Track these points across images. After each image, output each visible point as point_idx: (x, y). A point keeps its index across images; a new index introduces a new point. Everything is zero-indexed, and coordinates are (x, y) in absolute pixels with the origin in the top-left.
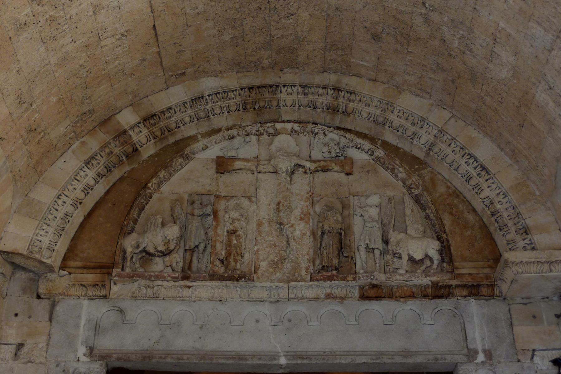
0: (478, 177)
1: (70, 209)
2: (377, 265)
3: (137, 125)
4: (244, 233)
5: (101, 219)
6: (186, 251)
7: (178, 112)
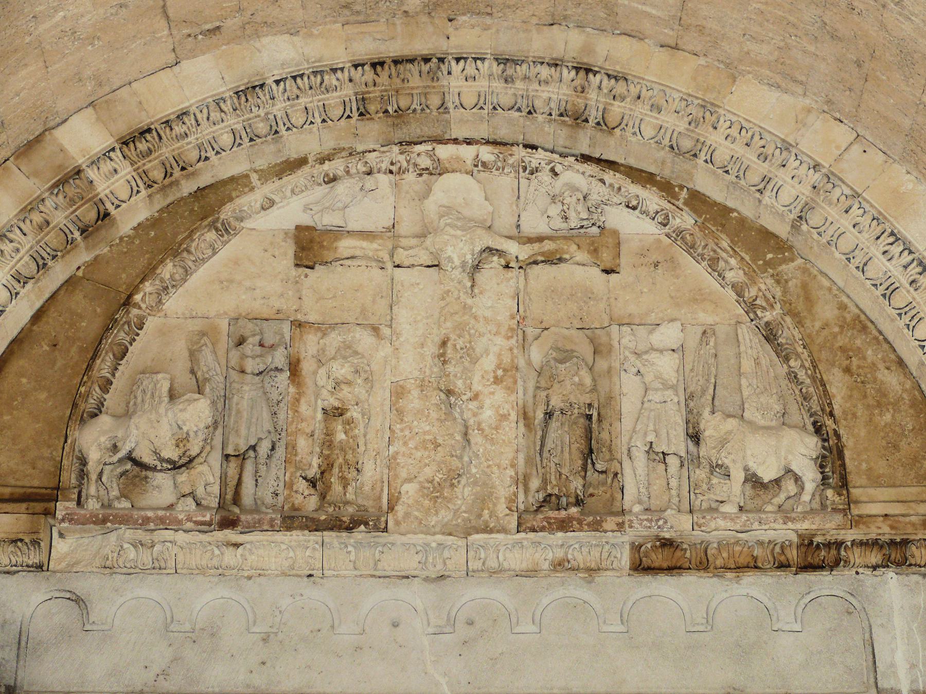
0: (912, 290)
3: (107, 154)
4: (363, 415)
5: (24, 380)
6: (227, 457)
7: (204, 123)
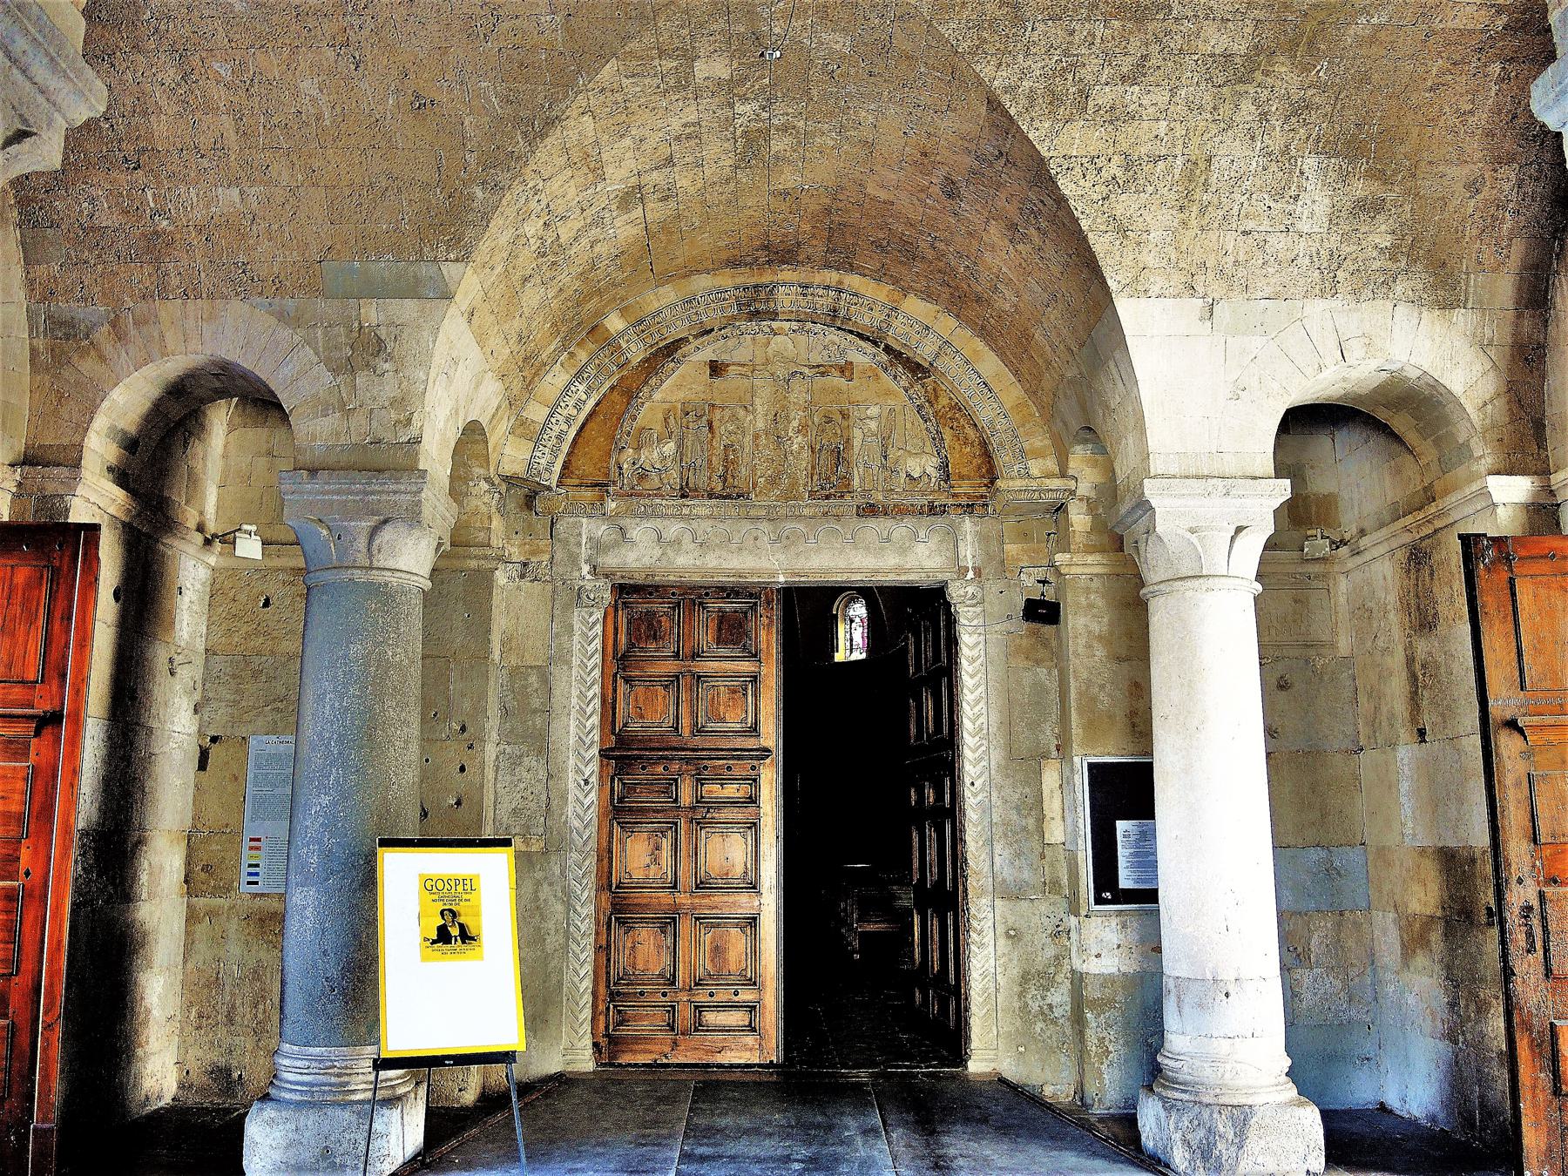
1: (564, 427)
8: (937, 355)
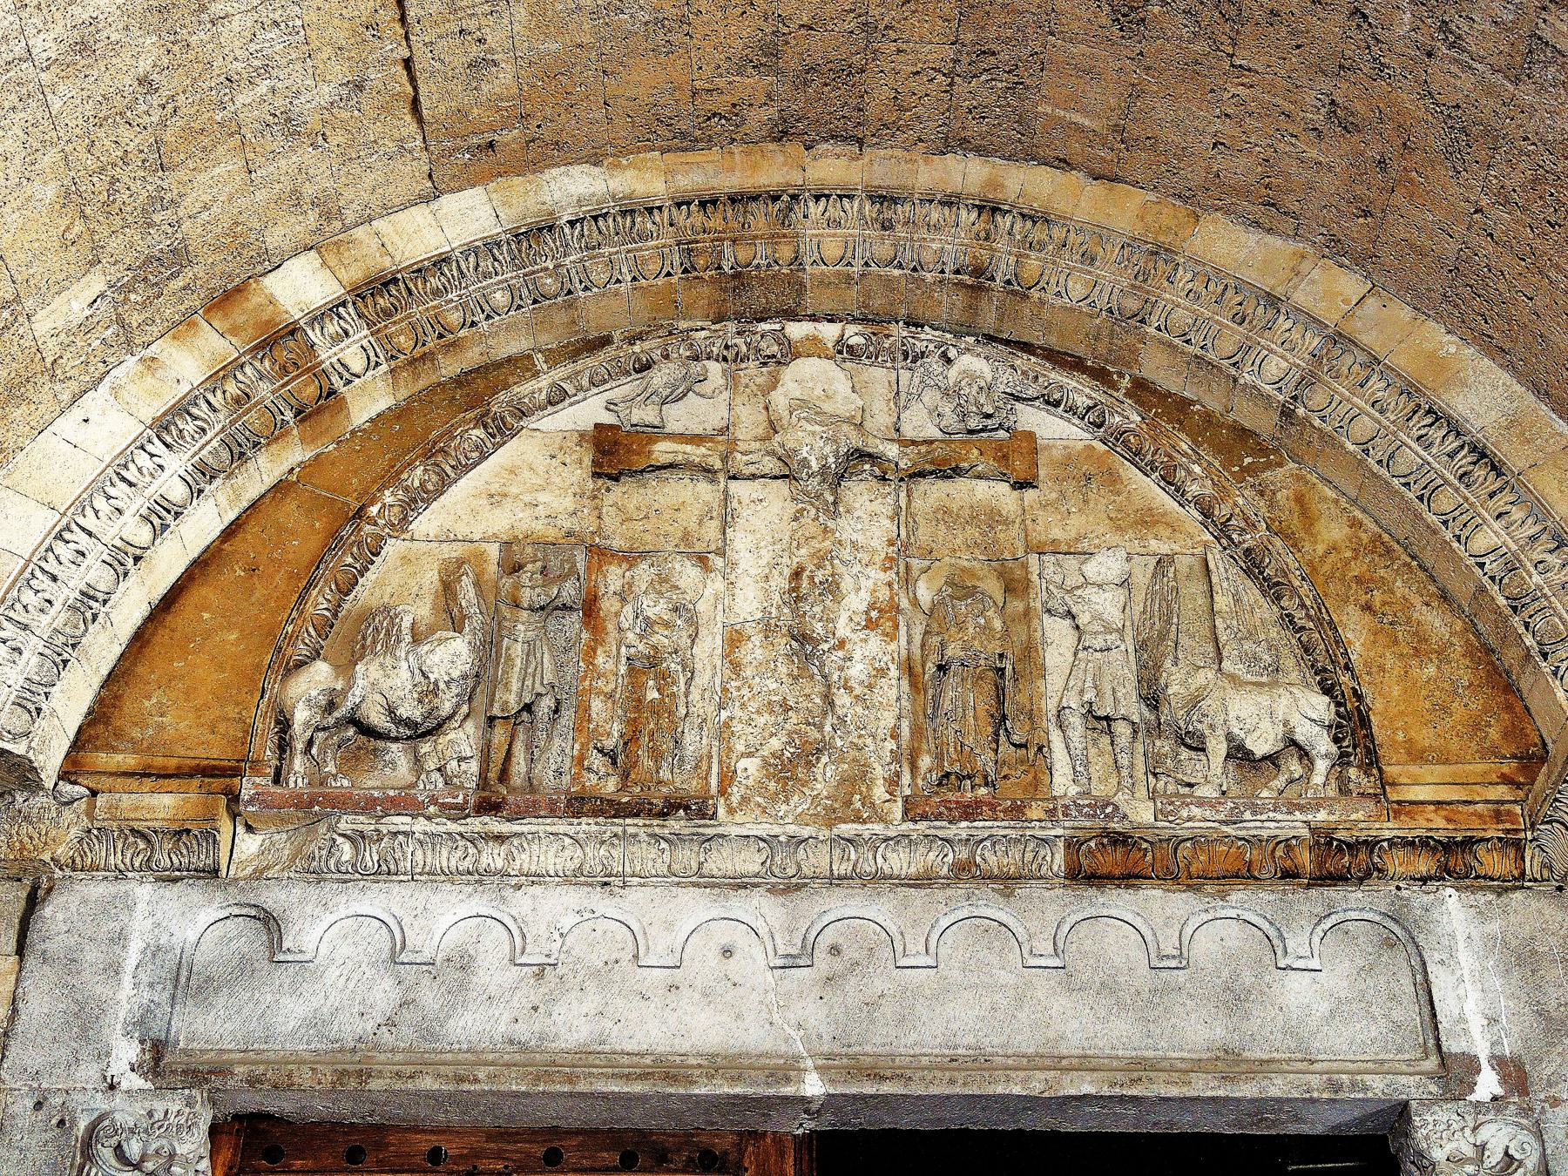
0: (1462, 488)
1: (101, 577)
2: (1125, 772)
5: (206, 616)
6: (491, 720)
7: (470, 274)
8: (1308, 380)
